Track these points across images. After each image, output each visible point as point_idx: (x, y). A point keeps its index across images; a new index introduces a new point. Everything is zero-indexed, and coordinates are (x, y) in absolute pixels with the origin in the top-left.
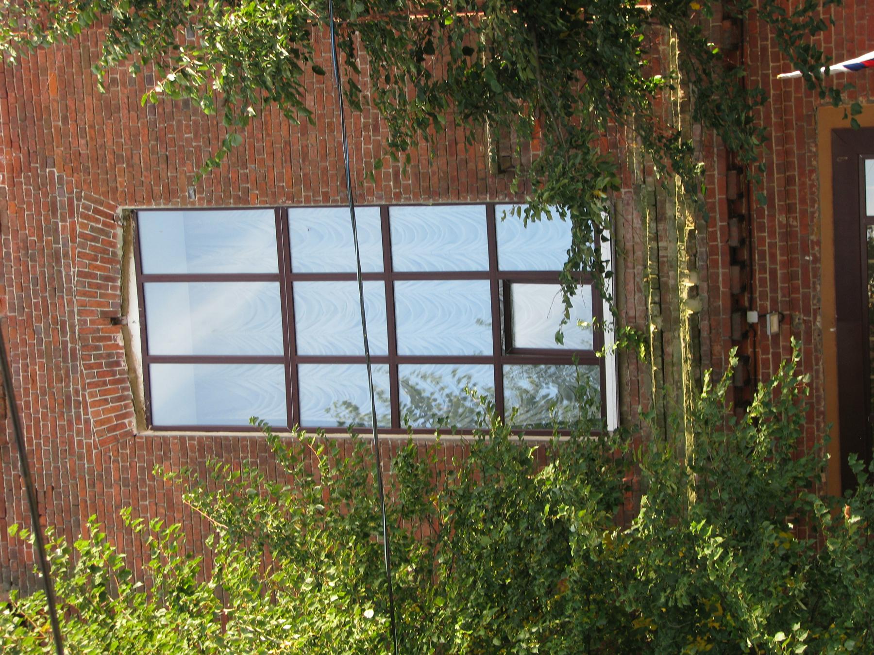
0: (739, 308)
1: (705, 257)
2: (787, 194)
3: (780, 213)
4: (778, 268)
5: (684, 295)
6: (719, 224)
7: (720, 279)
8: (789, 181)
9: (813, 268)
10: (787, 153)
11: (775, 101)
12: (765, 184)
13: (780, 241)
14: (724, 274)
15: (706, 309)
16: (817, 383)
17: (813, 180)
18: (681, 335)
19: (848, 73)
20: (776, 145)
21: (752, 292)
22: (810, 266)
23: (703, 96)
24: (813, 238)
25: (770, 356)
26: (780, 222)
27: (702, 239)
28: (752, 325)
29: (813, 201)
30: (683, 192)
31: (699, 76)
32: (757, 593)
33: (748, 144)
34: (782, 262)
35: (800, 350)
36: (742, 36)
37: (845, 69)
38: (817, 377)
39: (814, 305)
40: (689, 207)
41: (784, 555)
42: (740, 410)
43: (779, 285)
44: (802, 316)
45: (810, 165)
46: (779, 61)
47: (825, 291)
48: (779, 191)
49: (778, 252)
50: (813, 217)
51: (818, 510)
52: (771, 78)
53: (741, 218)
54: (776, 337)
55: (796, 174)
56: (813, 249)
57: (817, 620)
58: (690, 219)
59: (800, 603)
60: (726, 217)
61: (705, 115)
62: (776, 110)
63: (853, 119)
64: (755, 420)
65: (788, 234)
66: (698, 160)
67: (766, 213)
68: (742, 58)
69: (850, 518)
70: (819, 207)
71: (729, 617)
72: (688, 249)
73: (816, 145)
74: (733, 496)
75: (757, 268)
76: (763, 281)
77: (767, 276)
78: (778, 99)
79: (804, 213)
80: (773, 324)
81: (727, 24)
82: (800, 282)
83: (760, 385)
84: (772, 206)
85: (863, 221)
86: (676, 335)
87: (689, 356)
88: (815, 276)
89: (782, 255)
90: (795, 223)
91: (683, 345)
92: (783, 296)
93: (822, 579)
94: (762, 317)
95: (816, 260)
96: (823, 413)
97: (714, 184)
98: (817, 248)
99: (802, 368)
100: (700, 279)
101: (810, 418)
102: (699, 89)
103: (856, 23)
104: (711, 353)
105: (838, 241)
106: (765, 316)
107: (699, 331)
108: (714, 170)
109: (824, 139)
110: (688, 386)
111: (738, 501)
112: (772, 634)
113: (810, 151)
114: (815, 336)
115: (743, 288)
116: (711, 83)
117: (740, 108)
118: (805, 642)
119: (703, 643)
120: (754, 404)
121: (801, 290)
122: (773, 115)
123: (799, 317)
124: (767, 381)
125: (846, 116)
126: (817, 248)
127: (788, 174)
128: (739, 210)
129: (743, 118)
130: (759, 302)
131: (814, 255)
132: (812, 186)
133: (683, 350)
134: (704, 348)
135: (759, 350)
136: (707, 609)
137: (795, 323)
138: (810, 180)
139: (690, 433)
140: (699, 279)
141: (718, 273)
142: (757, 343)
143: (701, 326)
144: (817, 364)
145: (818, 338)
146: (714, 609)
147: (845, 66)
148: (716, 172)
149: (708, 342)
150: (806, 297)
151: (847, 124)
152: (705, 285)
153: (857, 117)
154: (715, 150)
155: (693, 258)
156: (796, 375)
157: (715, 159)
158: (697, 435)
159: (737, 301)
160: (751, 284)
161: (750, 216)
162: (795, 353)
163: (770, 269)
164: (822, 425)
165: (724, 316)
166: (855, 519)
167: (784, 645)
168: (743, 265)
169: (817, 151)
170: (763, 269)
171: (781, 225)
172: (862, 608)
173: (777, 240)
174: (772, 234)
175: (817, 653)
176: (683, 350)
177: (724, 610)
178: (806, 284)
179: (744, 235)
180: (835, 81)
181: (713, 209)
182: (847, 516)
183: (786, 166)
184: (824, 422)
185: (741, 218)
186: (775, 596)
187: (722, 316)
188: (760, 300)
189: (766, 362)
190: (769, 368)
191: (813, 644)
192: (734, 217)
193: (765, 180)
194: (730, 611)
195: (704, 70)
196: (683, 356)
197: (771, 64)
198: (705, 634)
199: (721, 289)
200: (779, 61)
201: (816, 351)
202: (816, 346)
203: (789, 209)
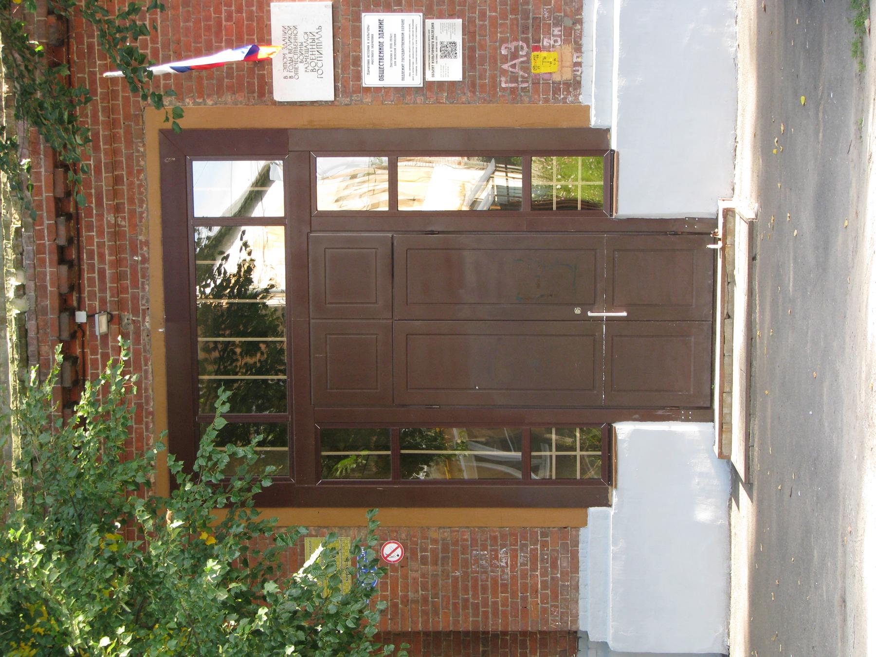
0: (66, 307)
1: (32, 256)
2: (115, 194)
3: (109, 213)
4: (107, 267)
5: (11, 294)
6: (46, 222)
7: (48, 278)
8: (117, 180)
9: (142, 269)
10: (115, 152)
11: (102, 99)
12: (93, 183)
13: (109, 241)
14: (52, 273)
15: (33, 308)
16: (146, 383)
17: (141, 180)
18: (8, 335)
19: (175, 74)
20: (104, 144)
21: (80, 292)
22: (139, 266)
23: (26, 92)
24: (141, 238)
25: (99, 356)
26: (108, 222)
27: (29, 237)
28: (80, 326)
29: (142, 201)
30: (9, 189)
31: (21, 71)
32: (82, 598)
33: (71, 144)
34: (111, 262)
35: (128, 349)
36: (68, 31)
37: (172, 71)
38: (146, 378)
39: (144, 305)
40: (15, 205)
41: (110, 557)
42: (68, 411)
43: (108, 285)
44: (131, 317)
45: (138, 165)
46: (106, 60)
47: (153, 292)
48: (107, 191)
49: (107, 252)
50: (141, 218)
51: (140, 516)
52: (98, 76)
53: (69, 217)
54: (105, 337)
55: (124, 173)
56: (141, 249)
57: (142, 620)
58: (17, 216)
59: (124, 606)
60: (53, 215)
61: (27, 113)
62: (102, 107)
63: (174, 122)
64: (83, 419)
65: (117, 234)
66: (22, 156)
67: (94, 212)
68: (68, 54)
69: (172, 522)
70: (147, 207)
71: (53, 622)
72: (14, 248)
73: (144, 145)
74: (59, 498)
75: (85, 267)
76: (91, 281)
77: (96, 275)
78: (106, 97)
79: (132, 213)
80: (102, 324)
81: (52, 19)
82: (129, 282)
83: (88, 385)
84: (99, 204)
85: (191, 222)
86: (3, 335)
87: (16, 356)
88: (143, 277)
89: (110, 255)
90: (123, 223)
91: (10, 345)
92: (112, 296)
93: (145, 580)
94: (91, 317)
95: (145, 260)
96: (152, 413)
97: (41, 182)
98: (145, 249)
99: (131, 369)
100: (27, 278)
101: (139, 421)
102: (21, 86)
103: (182, 24)
104: (39, 353)
105: (166, 241)
106: (94, 316)
107: (26, 330)
108: (40, 168)
109: (152, 139)
110: (14, 387)
111: (65, 502)
112: (98, 641)
113: (138, 151)
114: (143, 335)
115: (72, 288)
116: (34, 80)
117: (63, 106)
118: (129, 645)
119: (28, 649)
120: (81, 403)
121: (130, 291)
122: (100, 114)
123: (128, 317)
124: (95, 379)
125: (167, 119)
126: (145, 249)
127: (116, 173)
128: (65, 209)
129: (66, 117)
130: (87, 302)
131: (143, 256)
132: (140, 186)
133: (10, 350)
134: (32, 349)
135: (87, 350)
136: (32, 613)
137: (123, 324)
138: (138, 180)
139: (17, 435)
140: (26, 278)
141: (45, 272)
142: (86, 343)
143: (28, 326)
144: (146, 365)
145: (146, 339)
146: (39, 614)
147: (172, 68)
148: (43, 170)
149: (35, 342)
150: (135, 298)
151: (169, 125)
152: (32, 285)
153: (179, 121)
154: (42, 146)
155: (19, 256)
156: (123, 374)
157: (42, 156)
158: (24, 436)
159: (65, 301)
160: (79, 284)
161: (78, 214)
162: (123, 353)
163: (99, 269)
164: (151, 426)
165: (52, 316)
166: (177, 523)
167: (109, 650)
168: (71, 264)
169: (145, 150)
170: (92, 267)
171: (109, 225)
172: (185, 610)
173: (106, 240)
174: (101, 233)
175: (141, 654)
176: (10, 350)
177: (49, 614)
178: (135, 285)
179: (72, 234)
180: (162, 82)
181: (39, 207)
182: (169, 521)
183: (114, 166)
184: (153, 422)
185: (69, 217)
186: (98, 599)
187: (50, 316)
188: (89, 300)
189: (95, 362)
190: (98, 369)
191: (137, 645)
192: (62, 215)
193: (93, 179)
194: (54, 616)
195: (26, 67)
196: (10, 356)
197: (98, 62)
198: (29, 639)
199: (49, 288)
200: (106, 60)
201: (145, 351)
202: (145, 346)
203: (117, 209)
